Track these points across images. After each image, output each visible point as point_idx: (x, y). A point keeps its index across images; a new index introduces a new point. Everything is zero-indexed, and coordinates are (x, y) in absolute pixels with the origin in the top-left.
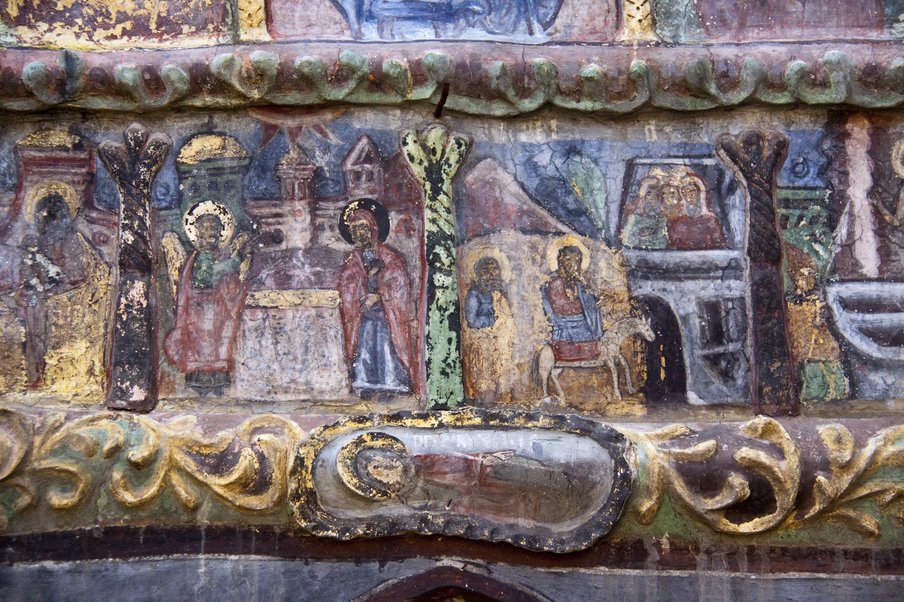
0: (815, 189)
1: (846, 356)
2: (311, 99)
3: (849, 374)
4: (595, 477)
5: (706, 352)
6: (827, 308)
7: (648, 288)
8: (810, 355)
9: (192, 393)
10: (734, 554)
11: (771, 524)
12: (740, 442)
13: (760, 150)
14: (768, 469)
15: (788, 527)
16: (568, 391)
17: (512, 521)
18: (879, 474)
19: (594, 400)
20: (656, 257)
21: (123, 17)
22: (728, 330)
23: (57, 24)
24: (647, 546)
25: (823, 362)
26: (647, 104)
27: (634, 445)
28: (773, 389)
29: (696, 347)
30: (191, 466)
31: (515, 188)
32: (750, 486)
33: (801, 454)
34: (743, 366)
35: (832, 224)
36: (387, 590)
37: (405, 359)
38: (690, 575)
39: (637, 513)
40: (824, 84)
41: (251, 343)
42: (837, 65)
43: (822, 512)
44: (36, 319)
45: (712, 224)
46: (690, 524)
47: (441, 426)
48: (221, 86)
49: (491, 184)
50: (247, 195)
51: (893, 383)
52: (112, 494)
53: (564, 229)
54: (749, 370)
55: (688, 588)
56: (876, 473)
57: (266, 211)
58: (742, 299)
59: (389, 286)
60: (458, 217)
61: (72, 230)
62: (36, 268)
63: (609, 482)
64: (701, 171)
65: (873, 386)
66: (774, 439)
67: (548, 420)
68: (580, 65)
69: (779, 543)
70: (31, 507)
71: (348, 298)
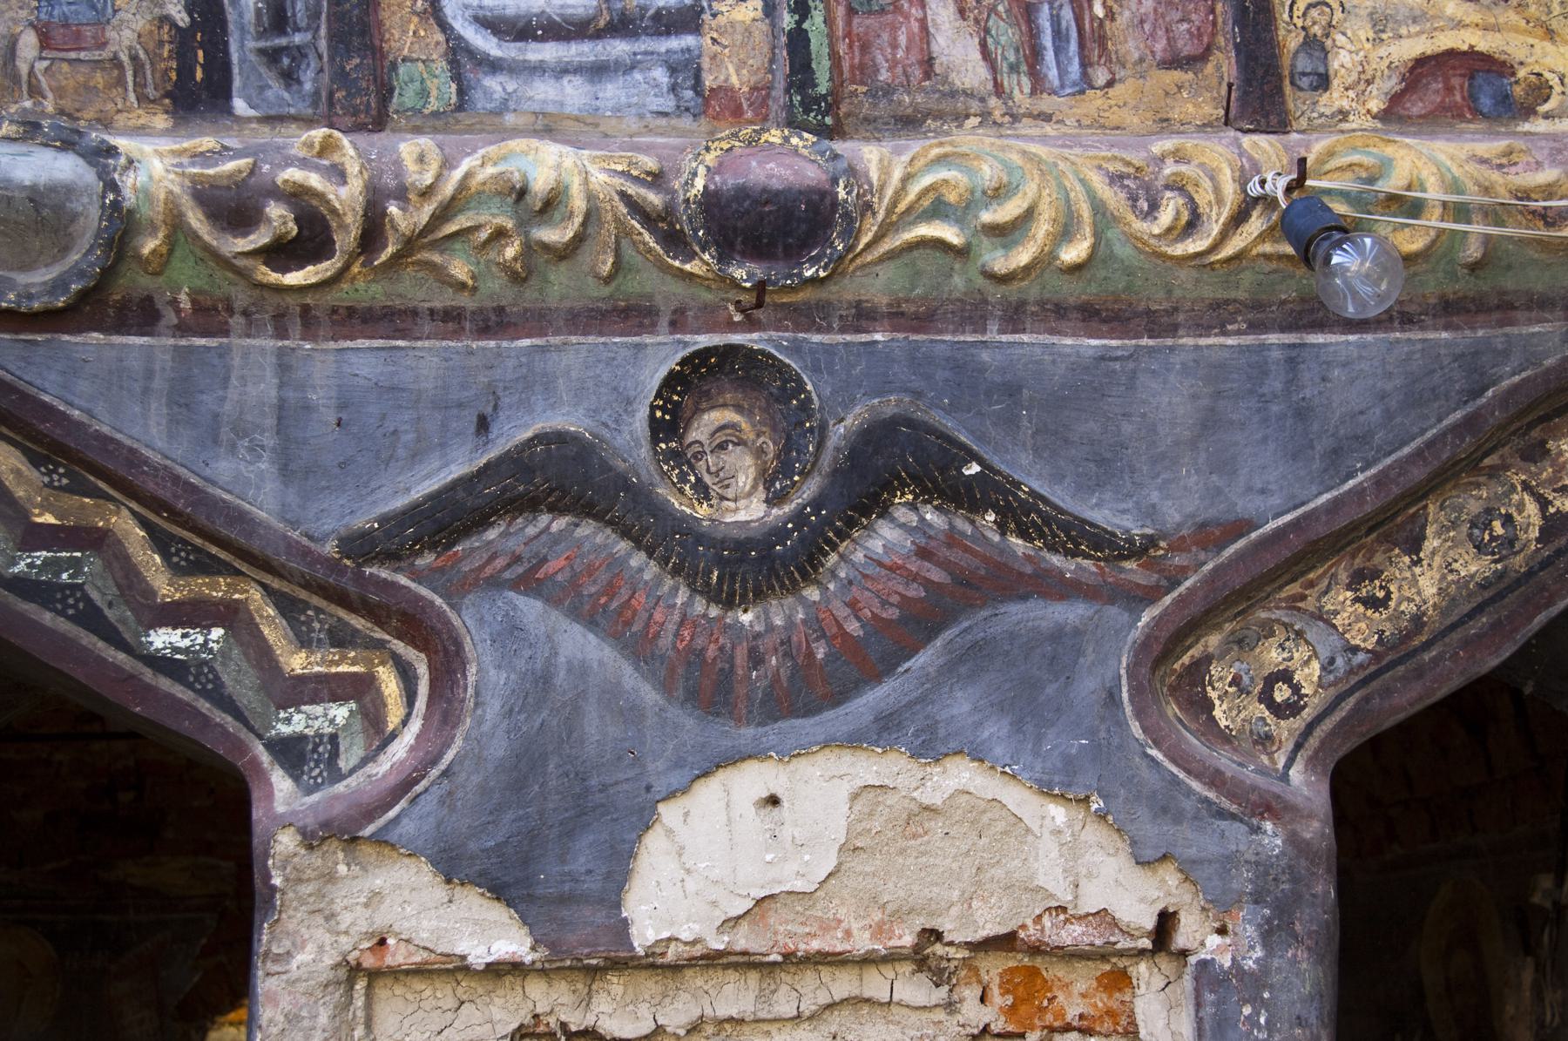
1: (454, 54)
3: (457, 77)
4: (76, 206)
5: (262, 44)
8: (406, 52)
10: (283, 315)
11: (329, 274)
12: (289, 162)
14: (321, 196)
15: (354, 279)
16: (60, 92)
18: (472, 205)
19: (98, 106)
22: (294, 15)
24: (159, 306)
25: (424, 62)
27: (136, 164)
28: (348, 95)
29: (249, 37)
32: (297, 220)
33: (370, 178)
34: (313, 65)
38: (221, 344)
39: (138, 257)
43: (397, 257)
46: (219, 274)
51: (515, 91)
54: (321, 70)
55: (216, 361)
56: (468, 202)
63: (94, 212)
65: (488, 94)
66: (336, 158)
67: (14, 128)
69: (343, 300)
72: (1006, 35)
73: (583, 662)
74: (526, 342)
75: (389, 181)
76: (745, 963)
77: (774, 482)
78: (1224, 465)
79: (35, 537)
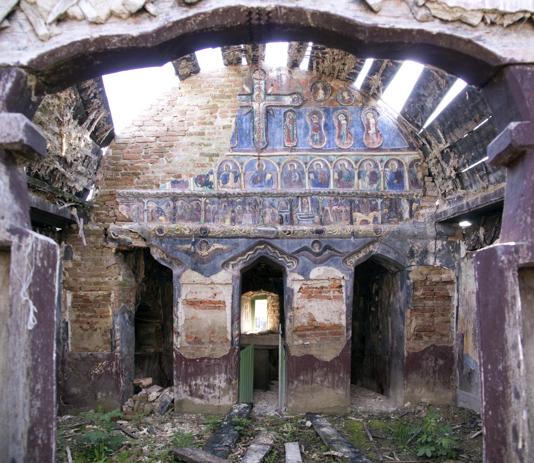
72: (335, 218)
76: (317, 280)
77: (319, 249)
78: (348, 248)
79: (272, 253)
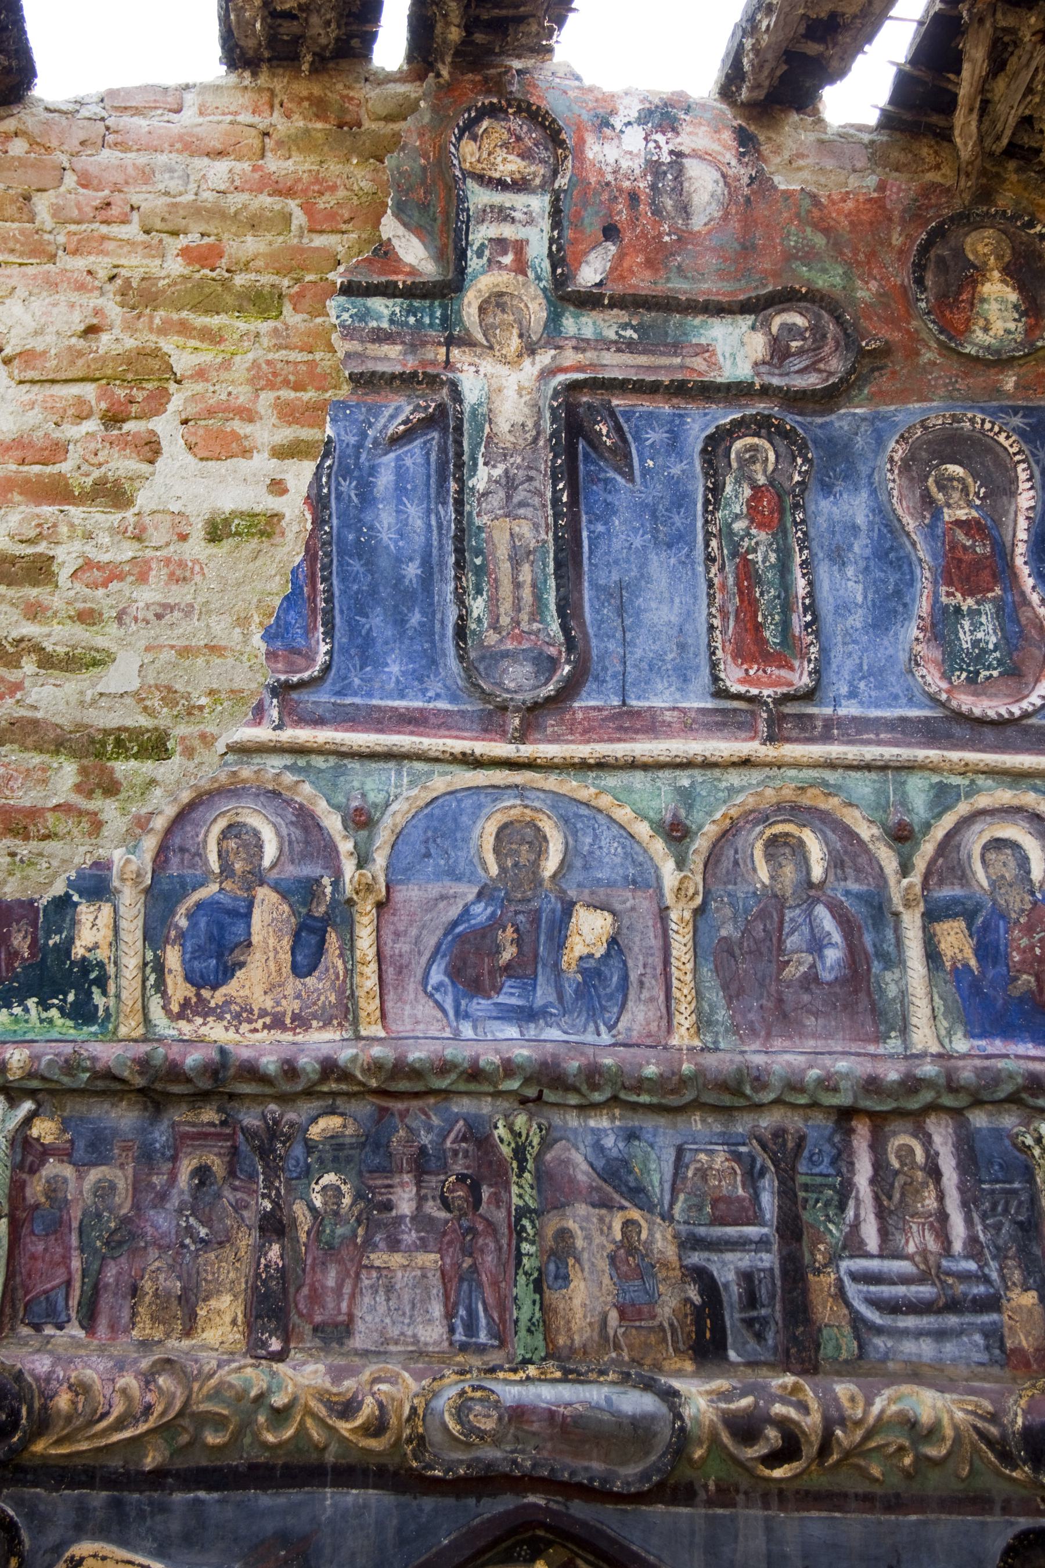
0: (828, 1176)
2: (419, 1087)
3: (858, 1337)
6: (840, 1280)
7: (696, 1258)
9: (318, 1343)
12: (773, 1399)
13: (784, 1144)
14: (797, 1424)
16: (631, 1347)
17: (586, 1464)
20: (702, 1231)
21: (263, 1013)
23: (210, 1019)
26: (695, 1100)
30: (323, 1412)
31: (585, 1167)
35: (842, 1207)
36: (482, 1523)
37: (496, 1316)
39: (690, 1460)
40: (836, 1090)
41: (367, 1299)
42: (846, 1076)
43: (838, 1463)
44: (189, 1275)
45: (747, 1204)
47: (528, 1378)
48: (345, 1076)
49: (567, 1163)
50: (364, 1168)
52: (256, 1435)
53: (626, 1204)
57: (379, 1182)
58: (772, 1269)
59: (482, 1251)
60: (539, 1192)
61: (219, 1196)
62: (189, 1230)
63: (668, 1432)
64: (737, 1157)
65: (876, 1348)
66: (801, 1396)
68: (641, 1066)
70: (190, 1444)
71: (448, 1261)
73: (20, 1371)
74: (913, 1517)
75: (835, 1414)
